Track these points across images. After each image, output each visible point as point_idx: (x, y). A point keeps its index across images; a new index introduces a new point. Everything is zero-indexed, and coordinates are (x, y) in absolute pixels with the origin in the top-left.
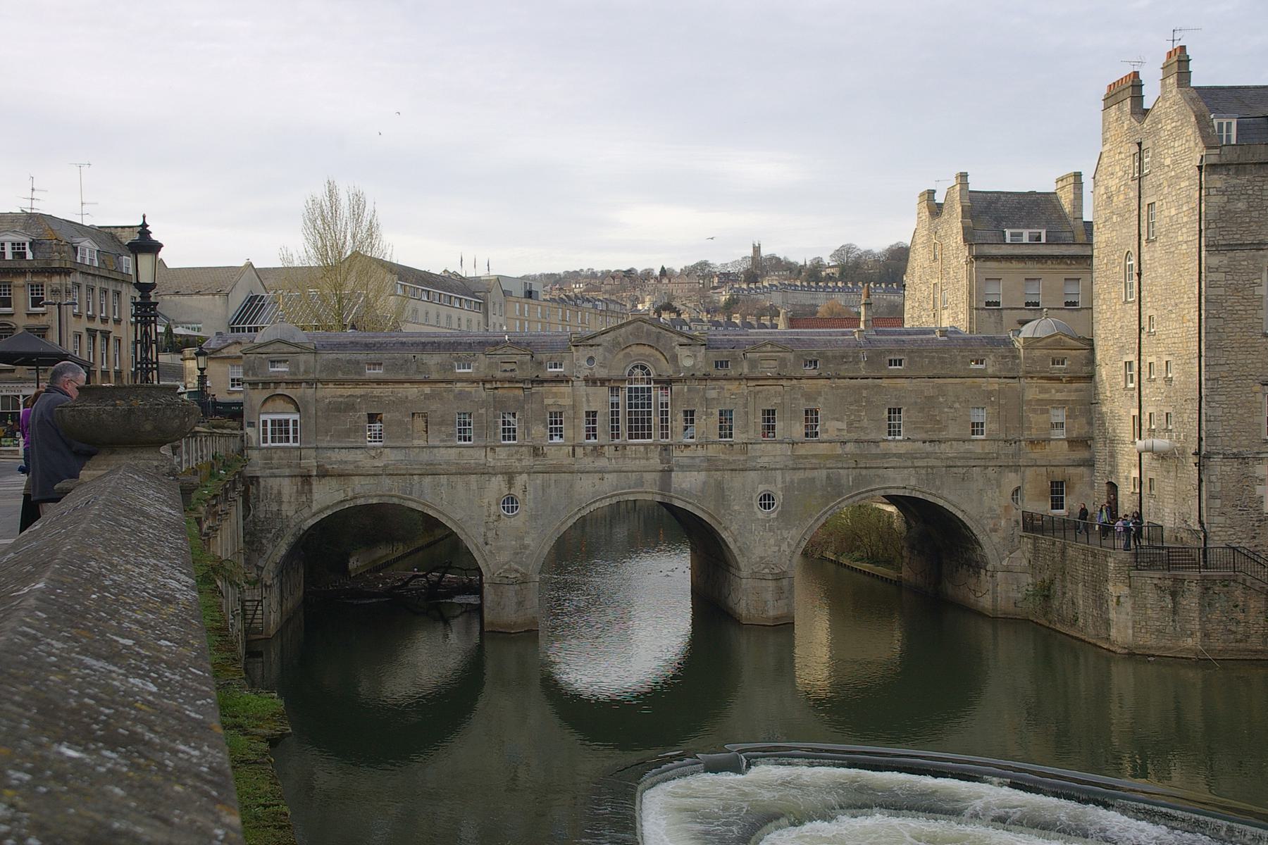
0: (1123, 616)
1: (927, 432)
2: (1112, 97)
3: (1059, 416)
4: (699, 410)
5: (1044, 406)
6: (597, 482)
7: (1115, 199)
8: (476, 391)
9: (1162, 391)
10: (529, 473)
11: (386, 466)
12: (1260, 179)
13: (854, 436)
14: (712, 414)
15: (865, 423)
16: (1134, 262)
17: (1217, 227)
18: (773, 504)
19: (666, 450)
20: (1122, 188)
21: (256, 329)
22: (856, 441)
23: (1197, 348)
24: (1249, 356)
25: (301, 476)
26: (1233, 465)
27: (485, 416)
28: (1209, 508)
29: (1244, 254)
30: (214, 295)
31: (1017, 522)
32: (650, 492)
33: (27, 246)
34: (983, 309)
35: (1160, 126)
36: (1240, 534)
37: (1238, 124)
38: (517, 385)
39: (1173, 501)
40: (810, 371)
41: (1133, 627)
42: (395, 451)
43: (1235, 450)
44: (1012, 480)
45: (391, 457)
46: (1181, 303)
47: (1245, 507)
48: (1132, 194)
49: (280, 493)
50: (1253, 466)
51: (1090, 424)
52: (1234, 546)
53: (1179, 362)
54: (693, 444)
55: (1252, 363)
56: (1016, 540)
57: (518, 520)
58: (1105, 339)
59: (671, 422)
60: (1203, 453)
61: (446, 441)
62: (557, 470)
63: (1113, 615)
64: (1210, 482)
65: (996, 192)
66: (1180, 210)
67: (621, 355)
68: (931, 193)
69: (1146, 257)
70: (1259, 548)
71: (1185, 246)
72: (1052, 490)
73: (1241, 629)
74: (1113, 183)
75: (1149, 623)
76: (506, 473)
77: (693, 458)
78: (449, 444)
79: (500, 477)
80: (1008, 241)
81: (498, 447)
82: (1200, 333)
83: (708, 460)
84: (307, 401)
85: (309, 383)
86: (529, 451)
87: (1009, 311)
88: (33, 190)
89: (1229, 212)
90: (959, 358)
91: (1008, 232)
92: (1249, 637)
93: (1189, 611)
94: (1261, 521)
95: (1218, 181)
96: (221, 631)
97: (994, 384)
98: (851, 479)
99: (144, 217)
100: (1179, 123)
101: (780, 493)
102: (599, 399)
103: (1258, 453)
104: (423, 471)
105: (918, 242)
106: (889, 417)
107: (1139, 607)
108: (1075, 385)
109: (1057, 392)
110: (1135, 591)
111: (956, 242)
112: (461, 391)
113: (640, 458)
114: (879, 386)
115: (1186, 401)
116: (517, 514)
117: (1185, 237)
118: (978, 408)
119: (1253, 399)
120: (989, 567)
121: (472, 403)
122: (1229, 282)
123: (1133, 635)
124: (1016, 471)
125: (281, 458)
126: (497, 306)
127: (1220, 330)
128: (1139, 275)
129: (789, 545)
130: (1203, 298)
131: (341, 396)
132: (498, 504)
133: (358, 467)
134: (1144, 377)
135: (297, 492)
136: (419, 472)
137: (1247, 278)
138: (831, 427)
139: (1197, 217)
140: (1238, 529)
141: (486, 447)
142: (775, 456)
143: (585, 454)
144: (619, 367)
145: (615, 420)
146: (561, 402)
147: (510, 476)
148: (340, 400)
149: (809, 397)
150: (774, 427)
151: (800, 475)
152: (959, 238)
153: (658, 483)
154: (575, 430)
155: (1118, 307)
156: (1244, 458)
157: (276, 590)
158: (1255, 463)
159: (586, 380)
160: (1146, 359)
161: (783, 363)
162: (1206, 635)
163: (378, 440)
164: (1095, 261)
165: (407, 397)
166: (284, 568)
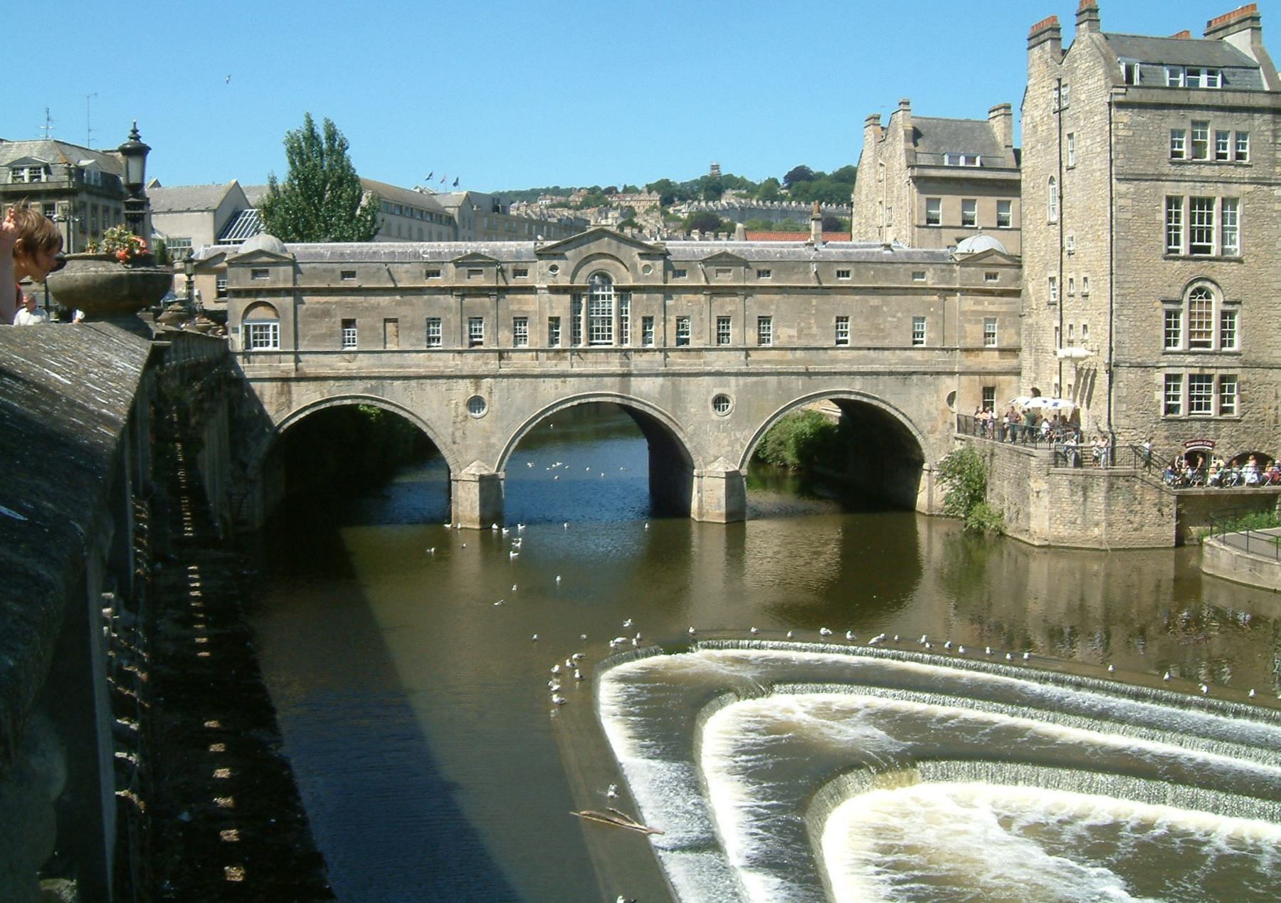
0: (1042, 510)
1: (871, 340)
2: (1036, 38)
4: (658, 317)
7: (1040, 129)
12: (1157, 117)
13: (803, 343)
14: (670, 320)
18: (727, 406)
20: (1045, 119)
23: (1109, 266)
24: (1152, 275)
26: (1137, 373)
28: (1117, 412)
30: (203, 211)
31: (952, 425)
32: (609, 391)
33: (42, 170)
34: (924, 227)
35: (1076, 65)
41: (1050, 519)
43: (1139, 360)
44: (950, 384)
45: (363, 364)
51: (1019, 334)
52: (1135, 445)
55: (1154, 281)
56: (951, 441)
58: (1032, 256)
60: (1113, 361)
63: (1032, 509)
69: (1066, 181)
70: (1155, 447)
73: (1137, 519)
74: (1037, 113)
77: (651, 362)
82: (1111, 252)
87: (957, 225)
88: (89, 130)
92: (1142, 526)
94: (1158, 423)
95: (1124, 116)
96: (103, 557)
100: (1092, 63)
101: (733, 396)
103: (1158, 362)
105: (865, 162)
107: (1055, 502)
110: (1053, 487)
123: (1050, 527)
128: (1061, 198)
129: (742, 446)
130: (1114, 221)
131: (318, 303)
135: (277, 393)
138: (782, 333)
139: (1109, 148)
140: (1139, 430)
148: (317, 306)
149: (762, 305)
154: (536, 336)
156: (1146, 367)
160: (1067, 275)
162: (1110, 525)
163: (351, 344)
164: (1023, 185)
165: (379, 304)
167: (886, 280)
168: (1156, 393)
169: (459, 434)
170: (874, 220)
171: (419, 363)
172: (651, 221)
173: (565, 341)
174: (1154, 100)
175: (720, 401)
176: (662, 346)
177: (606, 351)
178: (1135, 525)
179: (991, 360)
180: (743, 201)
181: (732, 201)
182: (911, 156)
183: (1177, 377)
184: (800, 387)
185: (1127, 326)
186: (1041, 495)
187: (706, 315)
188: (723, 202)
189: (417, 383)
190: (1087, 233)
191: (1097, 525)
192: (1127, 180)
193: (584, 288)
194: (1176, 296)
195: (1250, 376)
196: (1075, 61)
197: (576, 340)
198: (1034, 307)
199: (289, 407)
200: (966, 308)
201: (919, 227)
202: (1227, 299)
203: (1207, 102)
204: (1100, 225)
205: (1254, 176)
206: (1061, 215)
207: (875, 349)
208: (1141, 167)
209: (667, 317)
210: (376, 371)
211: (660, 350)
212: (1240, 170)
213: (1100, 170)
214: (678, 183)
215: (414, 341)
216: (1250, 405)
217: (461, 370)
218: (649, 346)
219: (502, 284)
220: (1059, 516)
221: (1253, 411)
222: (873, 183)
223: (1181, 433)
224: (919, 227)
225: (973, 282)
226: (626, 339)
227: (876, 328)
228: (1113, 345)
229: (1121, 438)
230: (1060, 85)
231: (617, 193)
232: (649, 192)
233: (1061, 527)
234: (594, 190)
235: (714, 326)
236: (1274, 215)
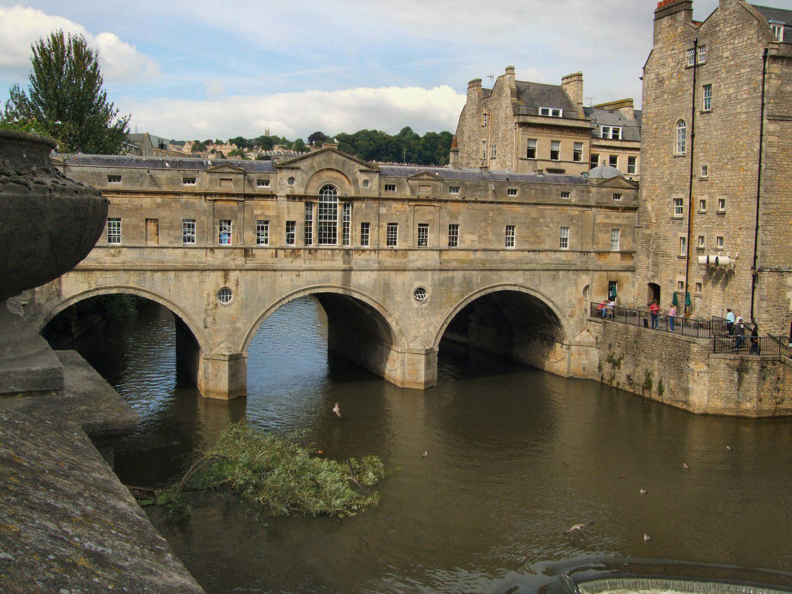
0: (702, 387)
1: (531, 244)
3: (617, 236)
4: (373, 223)
6: (294, 278)
7: (667, 82)
8: (199, 202)
9: (714, 220)
10: (241, 270)
11: (123, 263)
13: (482, 246)
14: (382, 226)
15: (490, 236)
16: (688, 127)
17: (774, 103)
18: (230, 297)
19: (347, 254)
20: (675, 75)
22: (485, 250)
24: (789, 199)
27: (206, 222)
29: (789, 124)
31: (586, 310)
34: (525, 159)
35: (718, 29)
36: (776, 325)
38: (232, 198)
39: (721, 300)
40: (455, 195)
41: (709, 395)
42: (131, 250)
43: (777, 266)
44: (585, 279)
45: (128, 256)
46: (738, 157)
47: (780, 306)
50: (786, 277)
53: (735, 200)
54: (368, 250)
56: (585, 323)
57: (229, 308)
59: (352, 232)
60: (758, 268)
61: (174, 242)
64: (761, 289)
65: (520, 82)
66: (739, 90)
68: (475, 83)
69: (700, 122)
72: (609, 288)
75: (720, 392)
76: (223, 270)
77: (367, 260)
78: (176, 245)
81: (217, 248)
89: (782, 92)
90: (554, 190)
91: (540, 109)
92: (783, 400)
93: (749, 383)
94: (787, 316)
95: (775, 68)
98: (479, 278)
100: (740, 26)
102: (296, 213)
104: (156, 268)
106: (507, 232)
107: (714, 380)
108: (627, 214)
109: (617, 218)
111: (506, 114)
112: (186, 201)
113: (327, 260)
115: (739, 229)
116: (231, 304)
117: (744, 110)
118: (564, 228)
119: (789, 229)
120: (566, 342)
121: (195, 212)
122: (780, 144)
123: (708, 400)
124: (587, 274)
126: (148, 151)
127: (773, 178)
128: (693, 136)
133: (99, 263)
134: (695, 211)
138: (466, 239)
139: (760, 94)
142: (427, 260)
143: (286, 256)
144: (314, 191)
145: (308, 230)
146: (268, 213)
147: (226, 271)
149: (453, 215)
151: (444, 274)
152: (508, 111)
153: (341, 279)
154: (276, 236)
155: (666, 159)
158: (788, 275)
161: (435, 190)
162: (760, 400)
165: (141, 206)
168: (787, 292)
169: (209, 320)
171: (174, 257)
173: (299, 241)
175: (420, 291)
176: (376, 247)
177: (332, 250)
178: (778, 400)
179: (615, 261)
180: (286, 151)
181: (280, 151)
182: (515, 107)
184: (479, 281)
185: (770, 239)
187: (410, 223)
188: (275, 151)
189: (175, 275)
190: (726, 164)
192: (775, 120)
193: (315, 197)
196: (718, 25)
197: (308, 241)
198: (654, 221)
201: (521, 159)
204: (744, 157)
206: (692, 149)
207: (534, 251)
208: (786, 111)
209: (381, 224)
210: (138, 264)
211: (375, 250)
213: (746, 113)
218: (365, 247)
219: (249, 191)
220: (717, 392)
222: (475, 128)
224: (521, 159)
226: (348, 241)
227: (535, 235)
228: (758, 254)
229: (762, 329)
230: (696, 46)
231: (213, 144)
232: (231, 144)
233: (719, 400)
234: (197, 142)
235: (416, 232)
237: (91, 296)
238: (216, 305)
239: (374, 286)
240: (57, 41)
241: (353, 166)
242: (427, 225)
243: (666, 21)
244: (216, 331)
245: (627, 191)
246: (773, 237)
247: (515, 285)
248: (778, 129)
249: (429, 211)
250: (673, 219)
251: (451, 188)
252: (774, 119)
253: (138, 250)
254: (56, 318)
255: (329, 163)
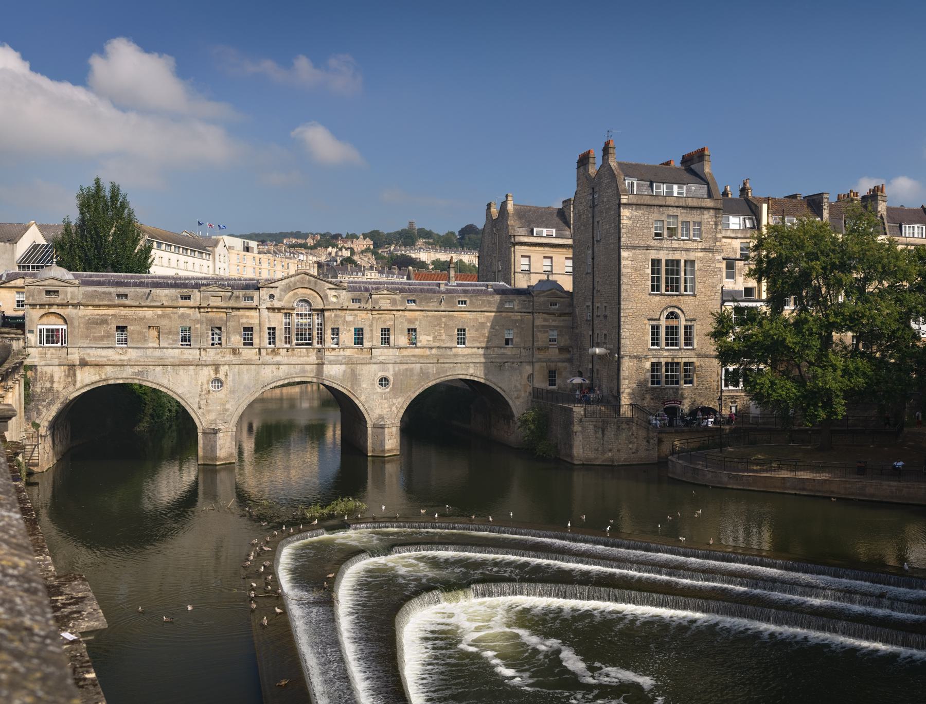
1: (480, 343)
4: (341, 328)
5: (545, 329)
6: (275, 370)
8: (193, 314)
11: (130, 360)
13: (437, 344)
14: (350, 330)
21: (38, 267)
25: (68, 366)
30: (5, 242)
31: (530, 393)
37: (637, 184)
41: (583, 448)
43: (635, 354)
44: (528, 369)
48: (590, 215)
49: (52, 376)
57: (221, 394)
62: (248, 363)
67: (291, 293)
69: (596, 249)
71: (612, 246)
74: (581, 208)
76: (214, 365)
79: (210, 368)
80: (535, 235)
83: (349, 357)
84: (73, 318)
85: (75, 306)
86: (230, 352)
92: (638, 451)
97: (518, 316)
99: (712, 314)
102: (278, 321)
104: (156, 363)
113: (303, 357)
114: (452, 316)
118: (509, 329)
125: (52, 354)
126: (222, 256)
128: (593, 259)
129: (397, 408)
131: (98, 315)
132: (208, 384)
135: (65, 375)
136: (153, 364)
137: (641, 264)
138: (424, 339)
141: (200, 349)
142: (389, 356)
143: (267, 354)
146: (251, 321)
147: (217, 367)
148: (97, 317)
149: (410, 321)
150: (389, 339)
151: (405, 367)
157: (49, 439)
159: (268, 309)
165: (145, 316)
166: (54, 426)
167: (489, 307)
169: (203, 402)
170: (491, 268)
172: (365, 259)
174: (645, 203)
175: (384, 381)
178: (634, 451)
181: (423, 247)
183: (659, 364)
184: (435, 372)
186: (577, 434)
189: (173, 369)
191: (610, 450)
194: (657, 317)
195: (702, 363)
199: (74, 385)
200: (538, 324)
202: (688, 318)
203: (676, 204)
205: (703, 247)
208: (637, 242)
212: (696, 243)
214: (386, 233)
215: (171, 342)
216: (702, 379)
217: (205, 361)
221: (704, 383)
223: (661, 396)
225: (543, 308)
231: (342, 238)
233: (590, 452)
234: (323, 236)
236: (715, 270)
237: (101, 385)
238: (209, 391)
239: (343, 375)
240: (82, 189)
241: (324, 285)
242: (650, 294)
243: (582, 169)
244: (209, 411)
245: (562, 300)
246: (631, 333)
247: (467, 375)
248: (631, 255)
249: (390, 318)
250: (587, 320)
251: (408, 301)
252: (628, 248)
253: (142, 350)
254: (71, 401)
255: (303, 283)
